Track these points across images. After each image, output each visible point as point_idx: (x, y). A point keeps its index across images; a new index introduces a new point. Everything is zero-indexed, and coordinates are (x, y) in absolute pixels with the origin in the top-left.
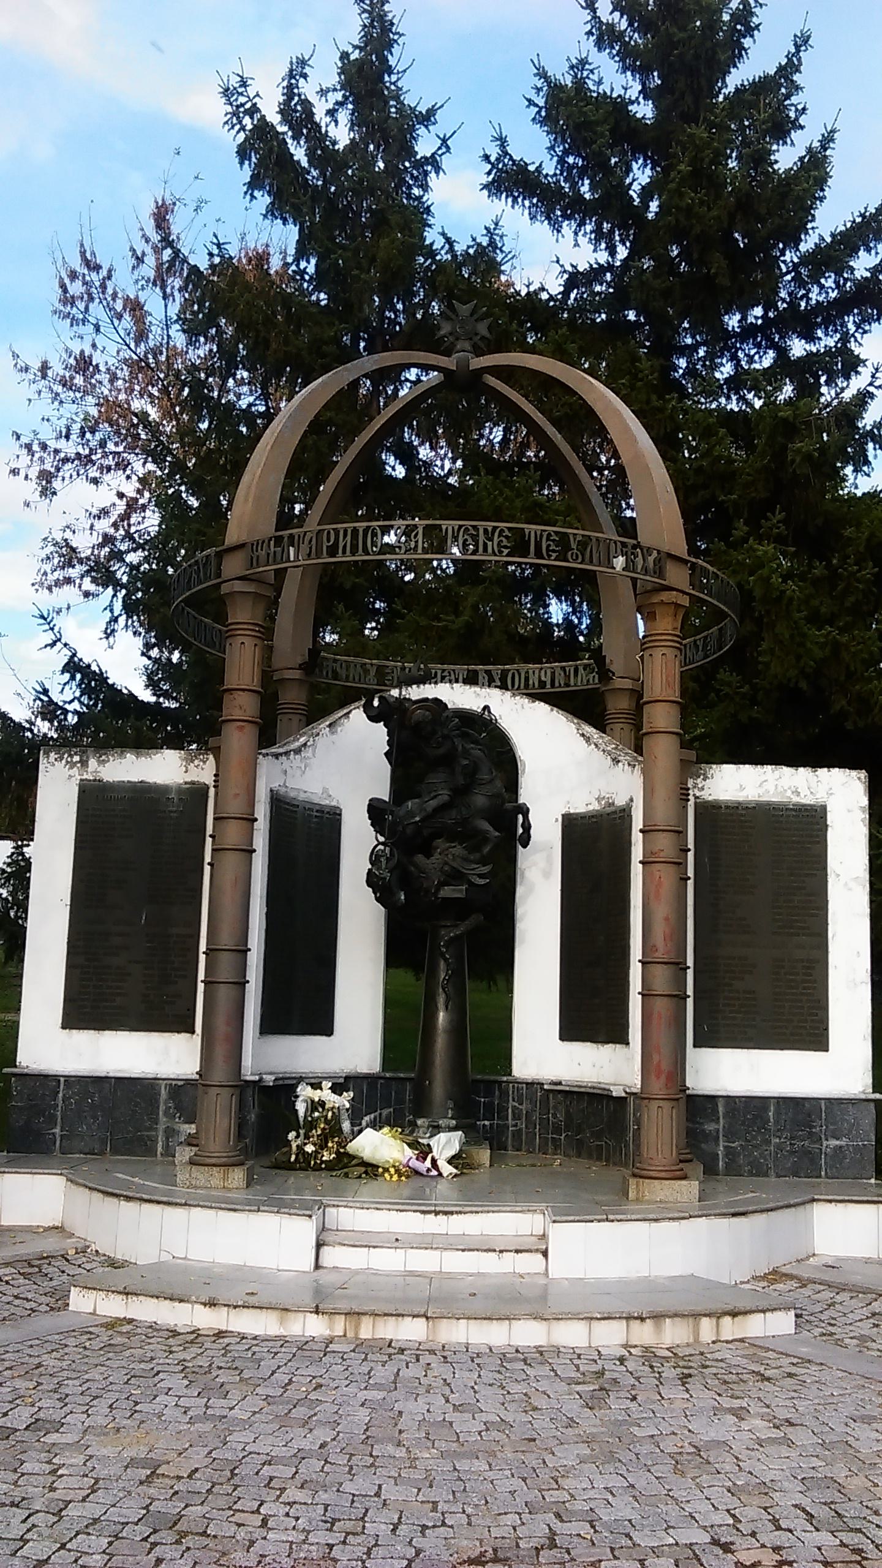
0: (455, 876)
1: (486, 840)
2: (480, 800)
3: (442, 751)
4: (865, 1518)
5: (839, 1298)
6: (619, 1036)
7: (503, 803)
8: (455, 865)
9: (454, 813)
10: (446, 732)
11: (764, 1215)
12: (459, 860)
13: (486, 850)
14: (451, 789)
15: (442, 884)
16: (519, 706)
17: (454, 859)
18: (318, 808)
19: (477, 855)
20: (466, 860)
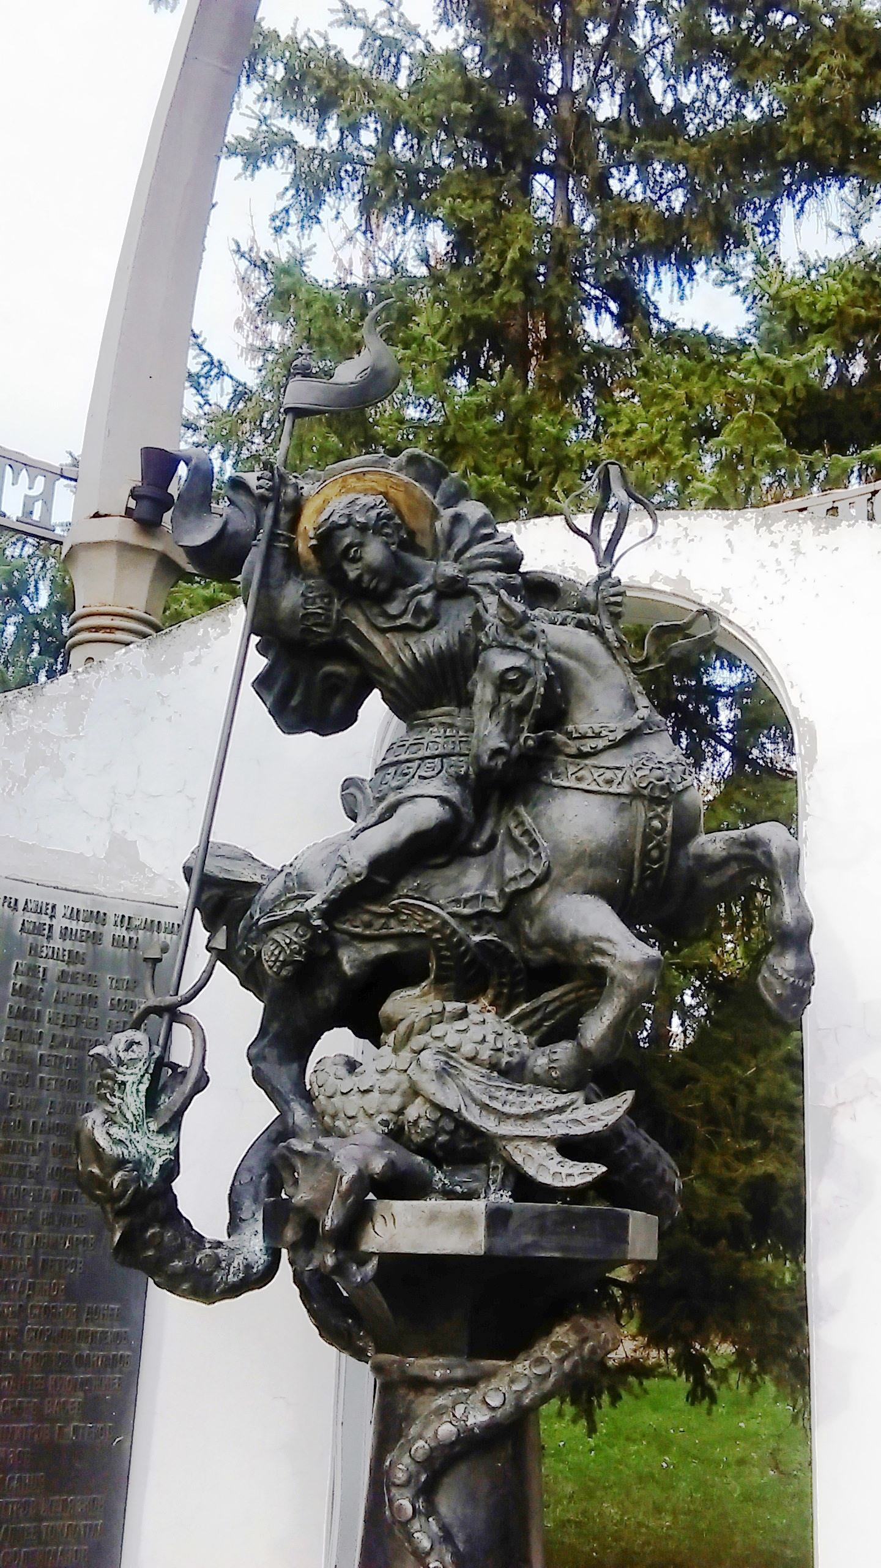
0: (451, 1151)
1: (597, 980)
2: (577, 816)
3: (436, 640)
4: (663, 43)
5: (510, 1097)
6: (626, 1218)
7: (685, 831)
8: (451, 1099)
9: (472, 878)
10: (449, 569)
11: (603, 796)
12: (472, 1074)
13: (596, 1028)
14: (460, 780)
15: (400, 1185)
16: (784, 552)
17: (444, 1073)
18: (81, 903)
19: (564, 1050)
20: (514, 1073)
